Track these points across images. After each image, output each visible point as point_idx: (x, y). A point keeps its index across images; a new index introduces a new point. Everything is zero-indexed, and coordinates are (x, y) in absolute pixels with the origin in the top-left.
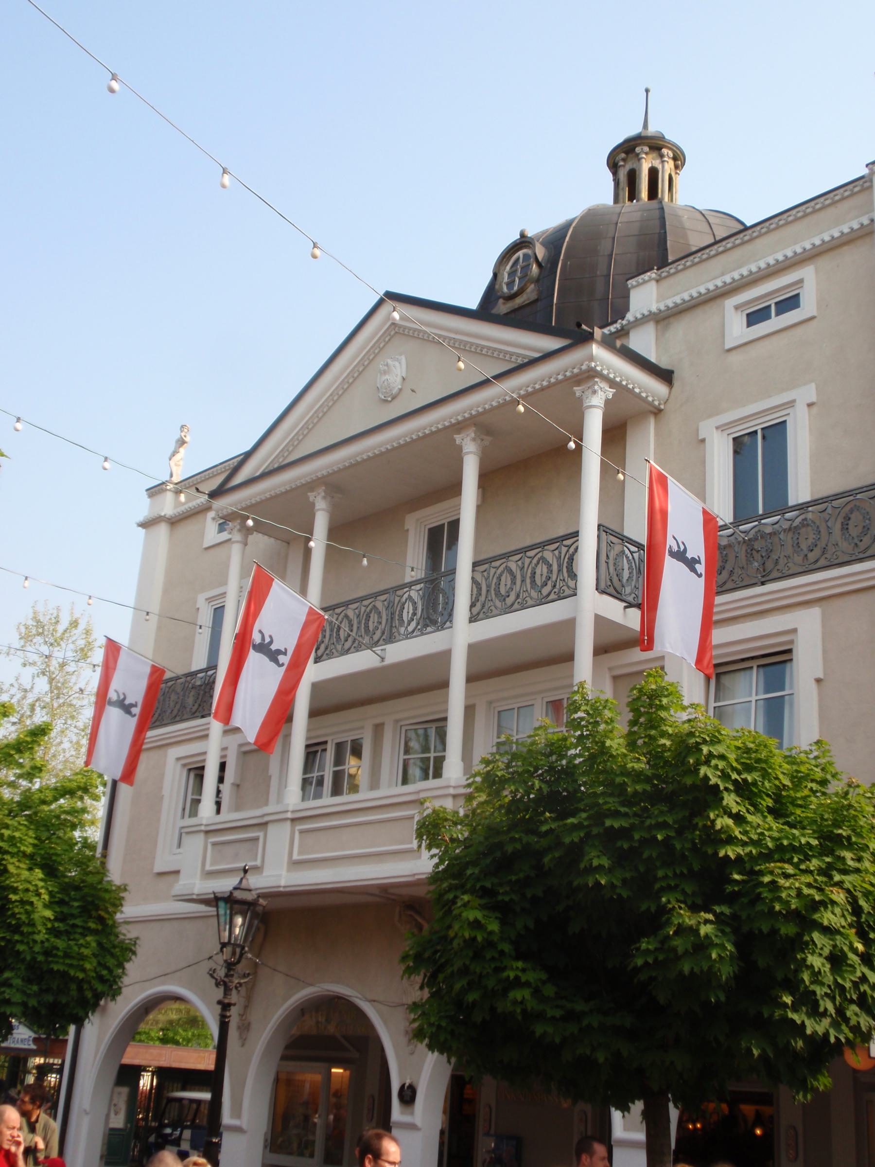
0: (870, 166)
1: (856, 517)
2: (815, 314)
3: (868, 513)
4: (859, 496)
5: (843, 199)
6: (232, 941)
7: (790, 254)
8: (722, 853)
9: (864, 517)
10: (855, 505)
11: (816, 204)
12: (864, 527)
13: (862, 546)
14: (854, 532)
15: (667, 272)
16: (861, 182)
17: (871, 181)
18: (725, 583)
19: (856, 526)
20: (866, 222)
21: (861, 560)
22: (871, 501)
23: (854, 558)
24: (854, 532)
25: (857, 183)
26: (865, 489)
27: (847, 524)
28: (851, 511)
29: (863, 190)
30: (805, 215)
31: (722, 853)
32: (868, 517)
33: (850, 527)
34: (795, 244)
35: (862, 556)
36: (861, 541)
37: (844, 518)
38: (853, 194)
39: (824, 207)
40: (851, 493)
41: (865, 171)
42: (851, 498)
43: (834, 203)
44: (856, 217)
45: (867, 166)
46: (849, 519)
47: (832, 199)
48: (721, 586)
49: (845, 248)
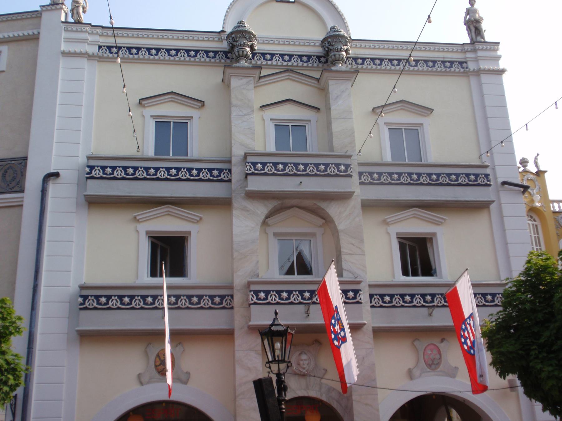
0: (42, 7)
1: (10, 172)
2: (63, 62)
3: (16, 171)
4: (13, 162)
5: (27, 18)
6: (276, 359)
7: (11, 35)
8: (523, 291)
9: (14, 172)
10: (10, 166)
11: (23, 15)
12: (13, 177)
13: (11, 186)
14: (8, 178)
15: (21, 17)
16: (36, 13)
17: (41, 14)
18: (14, 187)
19: (9, 176)
20: (36, 33)
21: (10, 193)
22: (18, 165)
23: (6, 191)
24: (8, 178)
25: (34, 13)
26: (16, 159)
27: (5, 175)
28: (8, 168)
29: (37, 17)
30: (7, 20)
31: (523, 291)
32: (16, 173)
33: (7, 176)
34: (35, 29)
35: (10, 190)
36: (11, 183)
37: (4, 171)
38: (32, 18)
39: (17, 20)
40: (9, 160)
41: (39, 9)
42: (9, 162)
43: (22, 19)
44: (32, 29)
45: (40, 6)
46: (7, 172)
47: (31, 15)
48: (11, 189)
49: (24, 42)
